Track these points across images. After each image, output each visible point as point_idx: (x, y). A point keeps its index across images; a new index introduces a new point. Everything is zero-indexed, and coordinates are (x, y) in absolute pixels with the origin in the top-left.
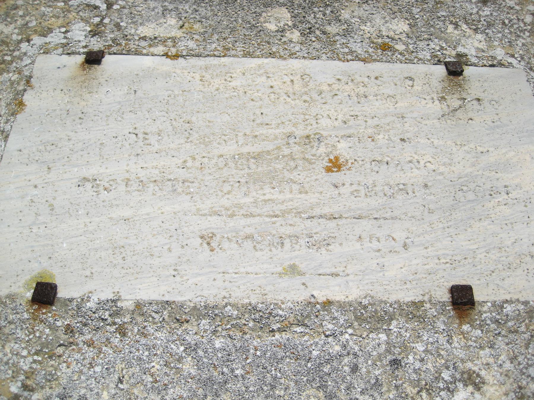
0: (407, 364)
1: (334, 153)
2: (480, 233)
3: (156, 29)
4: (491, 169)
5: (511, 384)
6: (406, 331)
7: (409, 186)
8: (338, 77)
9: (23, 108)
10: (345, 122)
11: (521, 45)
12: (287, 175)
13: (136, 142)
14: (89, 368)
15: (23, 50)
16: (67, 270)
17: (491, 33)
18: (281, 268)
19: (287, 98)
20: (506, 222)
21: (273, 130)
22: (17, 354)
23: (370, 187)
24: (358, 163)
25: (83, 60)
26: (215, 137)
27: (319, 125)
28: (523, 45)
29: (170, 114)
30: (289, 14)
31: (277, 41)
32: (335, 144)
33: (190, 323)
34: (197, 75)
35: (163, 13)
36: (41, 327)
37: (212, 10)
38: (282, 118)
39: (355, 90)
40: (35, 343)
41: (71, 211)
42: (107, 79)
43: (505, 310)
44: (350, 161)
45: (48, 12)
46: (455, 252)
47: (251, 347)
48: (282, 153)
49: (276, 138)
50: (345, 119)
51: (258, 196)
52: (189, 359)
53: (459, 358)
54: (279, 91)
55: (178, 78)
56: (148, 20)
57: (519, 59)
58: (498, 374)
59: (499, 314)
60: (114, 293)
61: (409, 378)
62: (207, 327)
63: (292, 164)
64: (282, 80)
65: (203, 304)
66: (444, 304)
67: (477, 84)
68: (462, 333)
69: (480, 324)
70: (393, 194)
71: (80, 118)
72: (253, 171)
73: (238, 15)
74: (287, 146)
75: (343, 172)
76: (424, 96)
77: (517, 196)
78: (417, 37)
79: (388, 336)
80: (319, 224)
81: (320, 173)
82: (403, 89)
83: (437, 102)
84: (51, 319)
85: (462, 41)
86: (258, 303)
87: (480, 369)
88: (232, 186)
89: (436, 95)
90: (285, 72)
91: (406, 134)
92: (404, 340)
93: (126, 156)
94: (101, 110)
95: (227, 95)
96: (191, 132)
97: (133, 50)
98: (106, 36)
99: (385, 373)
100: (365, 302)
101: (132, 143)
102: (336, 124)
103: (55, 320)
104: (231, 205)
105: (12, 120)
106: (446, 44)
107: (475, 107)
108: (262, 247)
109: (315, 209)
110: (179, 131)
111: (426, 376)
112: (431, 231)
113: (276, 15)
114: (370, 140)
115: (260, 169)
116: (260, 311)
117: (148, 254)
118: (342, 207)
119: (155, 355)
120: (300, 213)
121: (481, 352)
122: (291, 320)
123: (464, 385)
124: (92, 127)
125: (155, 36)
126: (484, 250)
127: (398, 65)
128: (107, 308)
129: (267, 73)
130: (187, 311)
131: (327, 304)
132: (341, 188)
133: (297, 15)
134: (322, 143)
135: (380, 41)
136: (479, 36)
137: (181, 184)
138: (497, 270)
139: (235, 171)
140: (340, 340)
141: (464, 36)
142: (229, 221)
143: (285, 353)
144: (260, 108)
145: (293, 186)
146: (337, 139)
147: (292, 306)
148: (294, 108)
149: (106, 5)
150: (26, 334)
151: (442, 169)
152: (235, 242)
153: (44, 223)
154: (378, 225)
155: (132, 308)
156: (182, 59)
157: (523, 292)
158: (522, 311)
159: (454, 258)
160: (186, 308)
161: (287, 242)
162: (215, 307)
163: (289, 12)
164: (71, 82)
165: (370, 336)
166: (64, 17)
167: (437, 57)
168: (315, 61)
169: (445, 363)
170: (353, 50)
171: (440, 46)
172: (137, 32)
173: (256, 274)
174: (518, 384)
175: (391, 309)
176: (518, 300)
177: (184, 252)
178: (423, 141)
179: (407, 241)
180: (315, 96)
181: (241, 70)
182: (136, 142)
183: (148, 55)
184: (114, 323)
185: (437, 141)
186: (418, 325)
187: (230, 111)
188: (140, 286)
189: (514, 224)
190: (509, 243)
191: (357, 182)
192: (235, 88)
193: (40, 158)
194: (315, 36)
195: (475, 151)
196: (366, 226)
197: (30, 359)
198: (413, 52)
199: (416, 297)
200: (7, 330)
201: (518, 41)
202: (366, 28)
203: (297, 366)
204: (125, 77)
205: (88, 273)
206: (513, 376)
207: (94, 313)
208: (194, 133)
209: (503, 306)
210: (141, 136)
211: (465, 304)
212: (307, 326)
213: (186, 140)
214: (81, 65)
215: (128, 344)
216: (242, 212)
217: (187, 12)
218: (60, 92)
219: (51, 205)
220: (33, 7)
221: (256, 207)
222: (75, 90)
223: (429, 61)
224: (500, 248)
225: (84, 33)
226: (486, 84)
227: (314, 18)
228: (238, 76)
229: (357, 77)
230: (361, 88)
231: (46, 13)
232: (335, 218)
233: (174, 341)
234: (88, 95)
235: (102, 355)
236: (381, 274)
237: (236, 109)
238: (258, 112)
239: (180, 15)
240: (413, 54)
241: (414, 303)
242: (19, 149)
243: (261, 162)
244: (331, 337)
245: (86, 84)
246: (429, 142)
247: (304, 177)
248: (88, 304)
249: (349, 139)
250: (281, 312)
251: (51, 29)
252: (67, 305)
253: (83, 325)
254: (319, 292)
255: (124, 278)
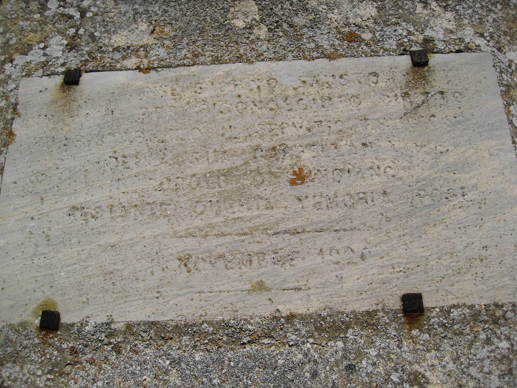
0: (361, 368)
1: (299, 164)
2: (433, 239)
3: (129, 37)
4: (450, 170)
5: (452, 383)
6: (361, 338)
7: (369, 194)
8: (303, 79)
9: (14, 138)
10: (309, 130)
11: (491, 21)
12: (255, 191)
13: (117, 166)
14: (93, 383)
15: (8, 73)
16: (66, 297)
17: (461, 9)
18: (249, 285)
19: (254, 107)
20: (459, 226)
21: (241, 144)
22: (33, 374)
23: (332, 198)
24: (321, 173)
25: (63, 81)
26: (188, 155)
27: (284, 135)
28: (494, 20)
29: (145, 134)
30: (256, 7)
31: (245, 40)
32: (299, 155)
33: (173, 340)
34: (168, 88)
35: (134, 18)
36: (50, 350)
37: (181, 10)
38: (250, 130)
39: (320, 93)
40: (47, 363)
41: (65, 241)
42: (86, 100)
43: (451, 315)
44: (313, 172)
45: (26, 26)
46: (409, 260)
47: (226, 358)
48: (250, 168)
49: (244, 152)
50: (309, 126)
51: (228, 215)
52: (174, 371)
53: (407, 361)
54: (247, 100)
55: (151, 94)
56: (121, 28)
57: (488, 38)
58: (442, 374)
59: (446, 318)
60: (108, 316)
61: (362, 381)
62: (188, 343)
63: (259, 178)
64: (249, 87)
65: (183, 323)
66: (396, 312)
67: (442, 74)
68: (412, 338)
69: (428, 328)
70: (353, 204)
71: (65, 145)
72: (223, 189)
73: (206, 13)
74: (254, 160)
75: (306, 184)
76: (387, 94)
77: (472, 198)
78: (384, 22)
79: (344, 343)
80: (284, 239)
81: (285, 186)
82: (367, 86)
83: (400, 99)
84: (57, 342)
85: (431, 22)
86: (230, 319)
87: (425, 371)
88: (205, 205)
89: (399, 91)
90: (251, 78)
91: (368, 138)
92: (359, 347)
93: (109, 181)
94: (83, 135)
95: (197, 109)
96: (165, 151)
97: (108, 65)
98: (82, 50)
99: (341, 377)
100: (324, 314)
101: (112, 168)
102: (301, 132)
103: (61, 343)
104: (204, 225)
105: (5, 151)
106: (414, 27)
107: (438, 102)
108: (233, 266)
109: (280, 225)
110: (155, 152)
111: (377, 379)
112: (387, 240)
113: (243, 10)
114: (333, 147)
115: (230, 186)
116: (232, 327)
117: (134, 278)
118: (305, 221)
119: (146, 369)
120: (266, 229)
121: (428, 355)
122: (259, 333)
123: (410, 386)
124: (76, 153)
125: (128, 45)
126: (436, 256)
127: (364, 60)
128: (103, 330)
129: (235, 81)
130: (170, 329)
131: (290, 318)
132: (304, 201)
133: (265, 8)
134: (287, 155)
135: (347, 29)
136: (449, 15)
137: (159, 208)
138: (448, 276)
139: (207, 190)
140: (302, 349)
141: (433, 15)
142: (202, 242)
143: (255, 363)
144: (229, 120)
145: (260, 202)
146: (301, 149)
147: (259, 321)
148: (260, 118)
149: (79, 13)
150: (39, 356)
151: (401, 174)
152: (209, 262)
153: (44, 254)
154: (337, 237)
155: (123, 329)
156: (154, 71)
157: (470, 296)
158: (467, 315)
159: (407, 266)
160: (168, 327)
161: (255, 259)
162: (194, 325)
163: (256, 4)
164: (53, 106)
165: (329, 344)
166: (41, 30)
167: (403, 45)
168: (281, 62)
169: (395, 366)
170: (320, 44)
171: (408, 30)
172: (111, 41)
173: (228, 292)
174: (458, 383)
175: (347, 319)
176: (464, 305)
177: (164, 274)
178: (384, 144)
179: (364, 251)
180: (281, 102)
181: (209, 79)
182: (117, 166)
183: (122, 70)
184: (110, 343)
185: (398, 143)
186: (372, 332)
187: (200, 127)
188: (129, 309)
189: (467, 227)
190: (460, 248)
191: (320, 194)
192: (205, 100)
193: (34, 189)
194: (283, 30)
195: (435, 151)
196: (327, 238)
197: (44, 378)
198: (379, 41)
199: (370, 307)
200: (23, 354)
201: (489, 17)
202: (333, 16)
203: (265, 374)
204: (102, 97)
205: (84, 299)
206: (455, 376)
207: (93, 335)
208: (168, 153)
209: (450, 311)
210: (120, 159)
211: (415, 311)
212: (273, 338)
213: (161, 160)
214: (61, 87)
215: (123, 361)
216: (215, 232)
217: (157, 15)
218: (45, 117)
219: (48, 236)
220: (12, 22)
221: (227, 226)
222: (58, 115)
223: (394, 51)
224: (452, 254)
225: (61, 48)
226: (451, 74)
227: (282, 9)
228: (207, 87)
229: (322, 77)
230: (326, 90)
231: (25, 28)
232: (298, 233)
233: (160, 357)
234: (70, 119)
235: (102, 371)
236: (339, 286)
237: (206, 124)
238: (227, 126)
239: (150, 19)
240: (380, 44)
241: (368, 312)
242: (14, 181)
243: (230, 179)
244: (294, 347)
245: (67, 107)
246: (390, 144)
247: (270, 192)
248: (86, 328)
249: (313, 147)
250: (250, 327)
251: (31, 45)
252: (70, 330)
253: (85, 347)
254: (283, 306)
255: (115, 302)
